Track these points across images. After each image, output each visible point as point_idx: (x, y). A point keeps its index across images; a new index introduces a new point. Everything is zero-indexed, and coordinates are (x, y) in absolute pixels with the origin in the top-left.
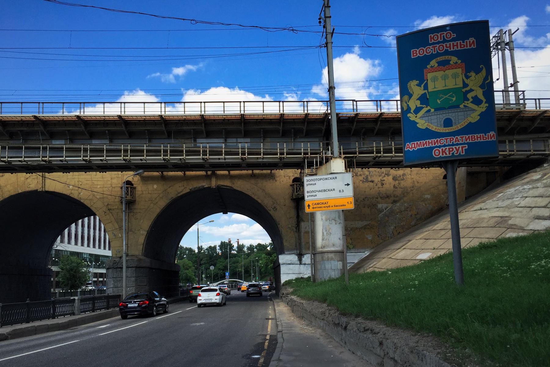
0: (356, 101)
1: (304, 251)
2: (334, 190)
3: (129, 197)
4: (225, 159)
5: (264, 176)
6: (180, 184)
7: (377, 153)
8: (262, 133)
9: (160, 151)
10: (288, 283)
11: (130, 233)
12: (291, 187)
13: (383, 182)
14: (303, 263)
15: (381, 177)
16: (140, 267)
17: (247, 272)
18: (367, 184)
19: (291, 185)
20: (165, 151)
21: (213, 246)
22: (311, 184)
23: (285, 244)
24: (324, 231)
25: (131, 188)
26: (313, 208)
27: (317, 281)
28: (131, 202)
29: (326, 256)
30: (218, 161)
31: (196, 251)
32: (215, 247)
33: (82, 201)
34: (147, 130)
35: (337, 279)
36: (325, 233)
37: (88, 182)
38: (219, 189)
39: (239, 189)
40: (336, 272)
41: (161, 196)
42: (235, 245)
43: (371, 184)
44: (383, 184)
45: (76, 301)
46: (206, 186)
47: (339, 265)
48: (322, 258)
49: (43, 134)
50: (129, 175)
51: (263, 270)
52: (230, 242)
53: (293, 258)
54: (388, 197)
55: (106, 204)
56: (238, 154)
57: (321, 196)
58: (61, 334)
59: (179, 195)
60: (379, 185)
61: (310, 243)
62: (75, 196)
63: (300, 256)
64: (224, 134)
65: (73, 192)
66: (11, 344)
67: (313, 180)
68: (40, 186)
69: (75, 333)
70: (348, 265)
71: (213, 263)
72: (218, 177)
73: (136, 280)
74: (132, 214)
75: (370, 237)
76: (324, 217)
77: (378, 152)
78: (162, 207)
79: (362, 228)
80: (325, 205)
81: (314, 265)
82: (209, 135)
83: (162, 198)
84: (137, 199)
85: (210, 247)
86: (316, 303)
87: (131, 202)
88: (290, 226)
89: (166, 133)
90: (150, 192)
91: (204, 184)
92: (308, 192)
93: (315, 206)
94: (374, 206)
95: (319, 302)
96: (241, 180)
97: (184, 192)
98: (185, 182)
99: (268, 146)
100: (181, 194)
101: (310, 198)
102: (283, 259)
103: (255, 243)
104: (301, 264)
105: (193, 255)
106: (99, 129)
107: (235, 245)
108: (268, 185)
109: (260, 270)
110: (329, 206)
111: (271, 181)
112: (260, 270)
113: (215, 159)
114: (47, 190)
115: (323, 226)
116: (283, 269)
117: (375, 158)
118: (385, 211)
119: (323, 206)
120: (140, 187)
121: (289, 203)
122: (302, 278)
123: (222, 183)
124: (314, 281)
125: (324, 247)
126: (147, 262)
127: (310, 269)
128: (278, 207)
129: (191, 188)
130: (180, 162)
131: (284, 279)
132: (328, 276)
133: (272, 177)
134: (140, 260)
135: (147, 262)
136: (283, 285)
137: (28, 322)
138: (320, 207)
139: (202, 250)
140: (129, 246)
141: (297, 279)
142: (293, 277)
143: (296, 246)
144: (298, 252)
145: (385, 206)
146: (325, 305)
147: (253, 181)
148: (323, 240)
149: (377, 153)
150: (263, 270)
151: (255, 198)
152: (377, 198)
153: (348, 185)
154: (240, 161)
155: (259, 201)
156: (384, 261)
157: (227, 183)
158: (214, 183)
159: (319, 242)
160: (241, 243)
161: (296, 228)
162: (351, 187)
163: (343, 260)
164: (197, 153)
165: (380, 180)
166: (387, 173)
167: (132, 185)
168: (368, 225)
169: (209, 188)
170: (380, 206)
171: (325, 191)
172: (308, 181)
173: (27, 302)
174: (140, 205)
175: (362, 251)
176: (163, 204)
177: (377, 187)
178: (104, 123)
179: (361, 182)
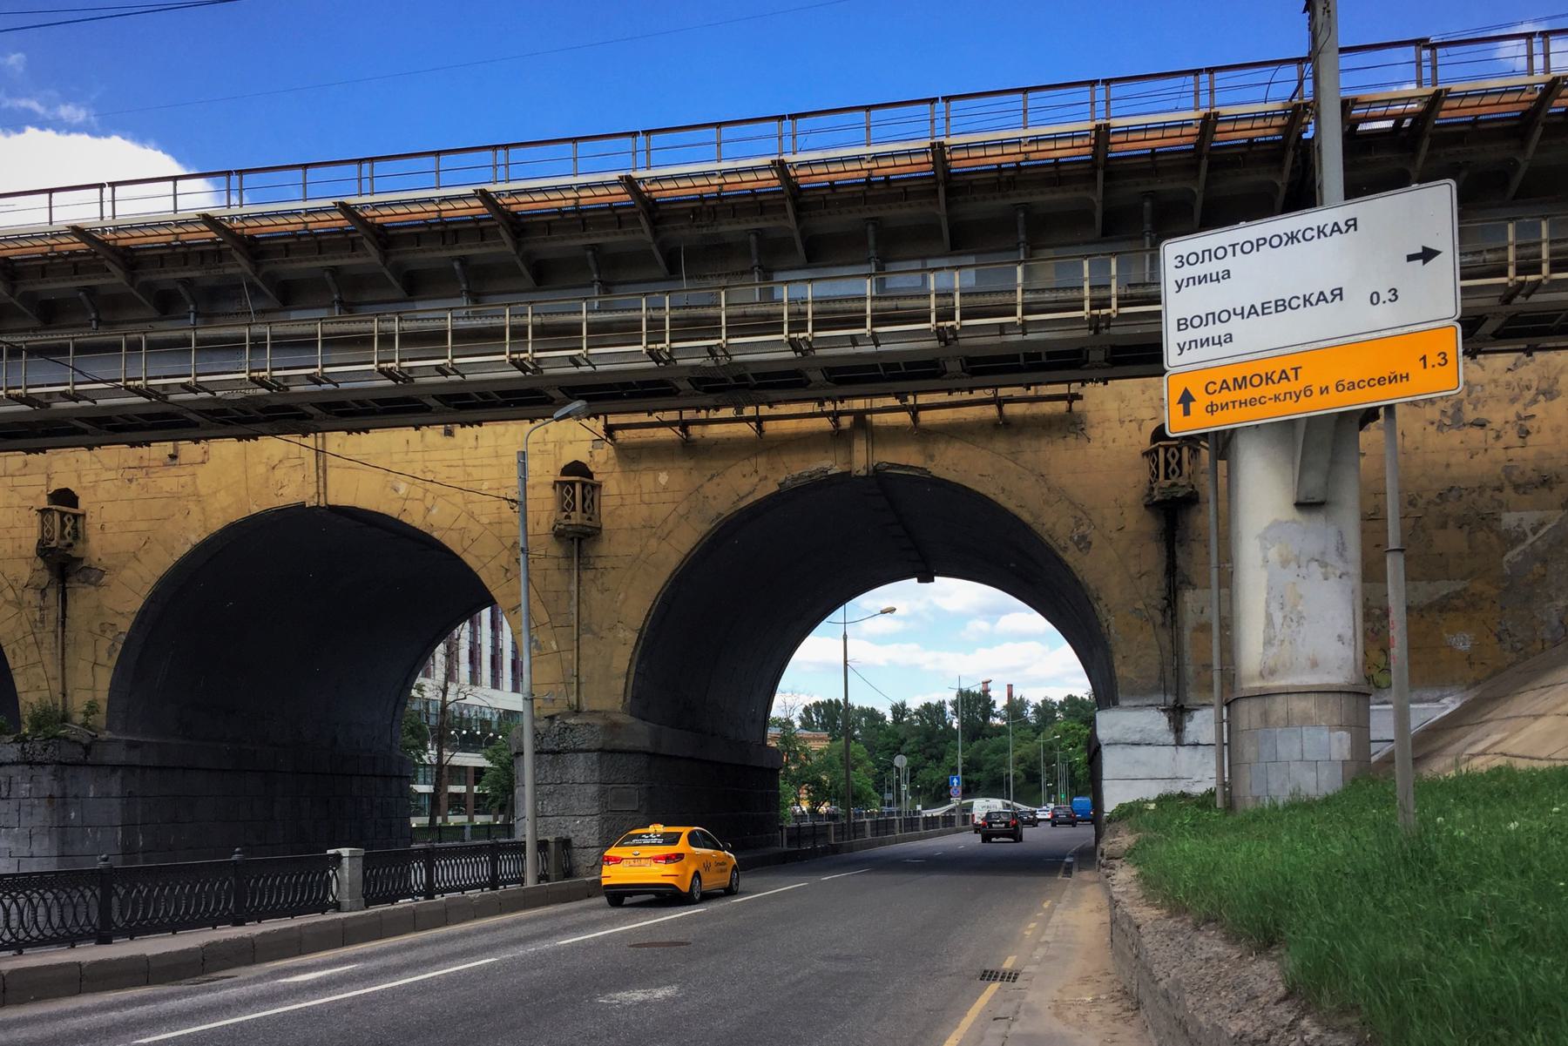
0: (1433, 47)
1: (1192, 698)
2: (1338, 293)
3: (577, 518)
4: (875, 339)
5: (1045, 426)
6: (747, 467)
7: (1520, 270)
8: (1021, 226)
9: (634, 326)
10: (1129, 812)
11: (586, 637)
12: (1146, 461)
13: (1528, 424)
14: (1189, 738)
15: (1518, 407)
16: (613, 751)
17: (1032, 777)
18: (1455, 437)
19: (1146, 454)
20: (656, 325)
21: (934, 702)
22: (1202, 279)
23: (1121, 671)
24: (1275, 607)
25: (584, 485)
26: (1212, 409)
27: (1239, 805)
28: (588, 535)
29: (1279, 706)
30: (851, 350)
31: (889, 718)
32: (940, 708)
33: (435, 535)
34: (593, 247)
35: (1327, 801)
36: (1278, 617)
37: (454, 472)
38: (879, 476)
39: (951, 476)
40: (1325, 774)
41: (682, 510)
42: (1000, 701)
43: (1476, 433)
44: (1524, 433)
45: (346, 862)
46: (836, 470)
47: (1335, 746)
48: (1265, 716)
49: (256, 292)
50: (571, 437)
51: (1080, 772)
52: (986, 691)
53: (1154, 722)
54: (1546, 482)
55: (509, 543)
56: (860, 323)
57: (1256, 339)
58: (142, 1001)
59: (743, 504)
60: (1511, 436)
61: (1216, 666)
62: (415, 519)
63: (1178, 714)
64: (871, 242)
65: (408, 505)
66: (38, 1020)
67: (1211, 254)
68: (312, 490)
69: (221, 994)
70: (1374, 747)
71: (935, 751)
72: (876, 436)
73: (602, 794)
74: (590, 574)
75: (1462, 643)
76: (1273, 554)
77: (1529, 265)
78: (686, 549)
79: (1430, 606)
80: (1284, 387)
81: (1228, 747)
82: (819, 252)
83: (685, 516)
84: (606, 523)
85: (927, 706)
86: (1211, 944)
87: (588, 535)
88: (1140, 605)
89: (661, 262)
90: (646, 498)
91: (826, 464)
92: (1182, 324)
93: (1219, 399)
94: (1487, 520)
95: (1232, 938)
96: (958, 445)
97: (758, 495)
98: (762, 461)
99: (1049, 273)
100: (750, 500)
101: (1192, 355)
102: (1109, 724)
103: (1058, 696)
104: (1179, 743)
105: (880, 728)
106: (429, 255)
107: (1000, 701)
108: (1059, 456)
109: (1072, 774)
110: (1308, 391)
111: (1071, 440)
112: (1072, 774)
113: (836, 344)
114: (331, 502)
115: (1270, 589)
116: (1112, 762)
117: (1508, 295)
118: (1531, 539)
119: (1269, 390)
120: (613, 482)
121: (1138, 521)
122: (1183, 795)
123: (888, 456)
124: (1230, 806)
125: (1272, 672)
126: (640, 734)
127: (1213, 764)
128: (1094, 536)
129: (782, 479)
130: (711, 363)
131: (1114, 796)
132: (1289, 787)
133: (1072, 425)
134: (612, 728)
135: (640, 734)
136: (1110, 820)
137: (239, 922)
138: (1252, 402)
139: (903, 715)
140: (583, 680)
141: (1162, 800)
142: (1151, 791)
143: (1162, 679)
144: (1171, 700)
145: (1530, 517)
146: (1266, 975)
147: (1001, 445)
148: (1268, 642)
149: (1520, 270)
150: (1080, 772)
151: (1011, 505)
152: (1500, 489)
153: (1427, 255)
154: (932, 344)
155: (1026, 517)
156: (1539, 726)
157: (908, 456)
158: (861, 459)
159: (1253, 652)
160: (1016, 695)
161: (1164, 612)
162: (1446, 266)
163: (1359, 729)
164: (770, 324)
165: (1512, 417)
166: (1544, 386)
167: (590, 475)
168: (1458, 595)
169: (845, 476)
170: (1509, 519)
171: (1282, 305)
172: (1182, 261)
173: (235, 857)
174: (614, 548)
175: (1428, 694)
176: (686, 539)
177: (1501, 444)
178: (443, 233)
179: (1432, 429)
